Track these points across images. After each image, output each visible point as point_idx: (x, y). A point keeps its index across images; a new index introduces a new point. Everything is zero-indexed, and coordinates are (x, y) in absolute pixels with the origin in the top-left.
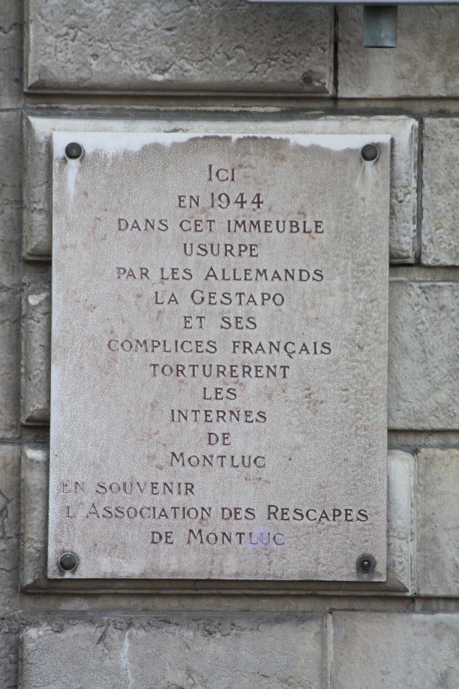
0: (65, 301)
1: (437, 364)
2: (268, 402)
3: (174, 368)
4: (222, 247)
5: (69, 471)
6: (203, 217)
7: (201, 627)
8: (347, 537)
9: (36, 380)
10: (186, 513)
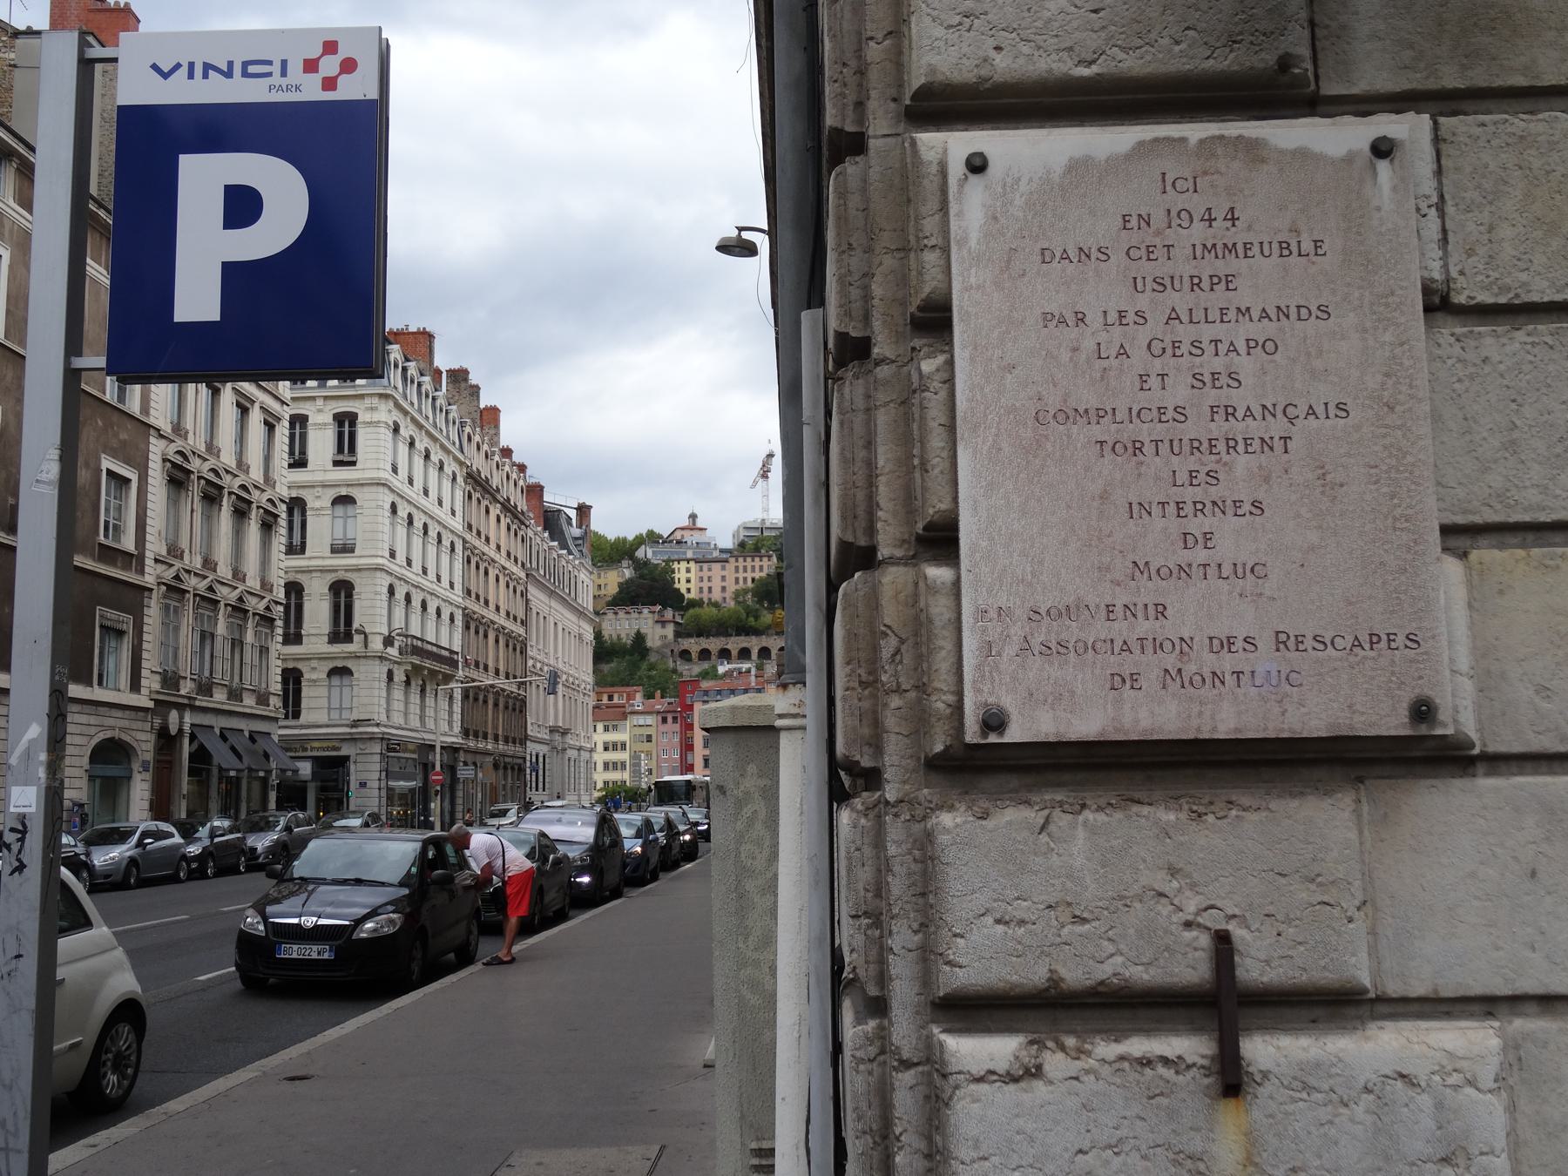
0: (972, 360)
1: (1485, 434)
2: (1265, 487)
3: (1129, 445)
4: (1186, 280)
5: (989, 591)
6: (1158, 241)
7: (1186, 807)
8: (1393, 673)
9: (937, 471)
10: (1158, 646)
